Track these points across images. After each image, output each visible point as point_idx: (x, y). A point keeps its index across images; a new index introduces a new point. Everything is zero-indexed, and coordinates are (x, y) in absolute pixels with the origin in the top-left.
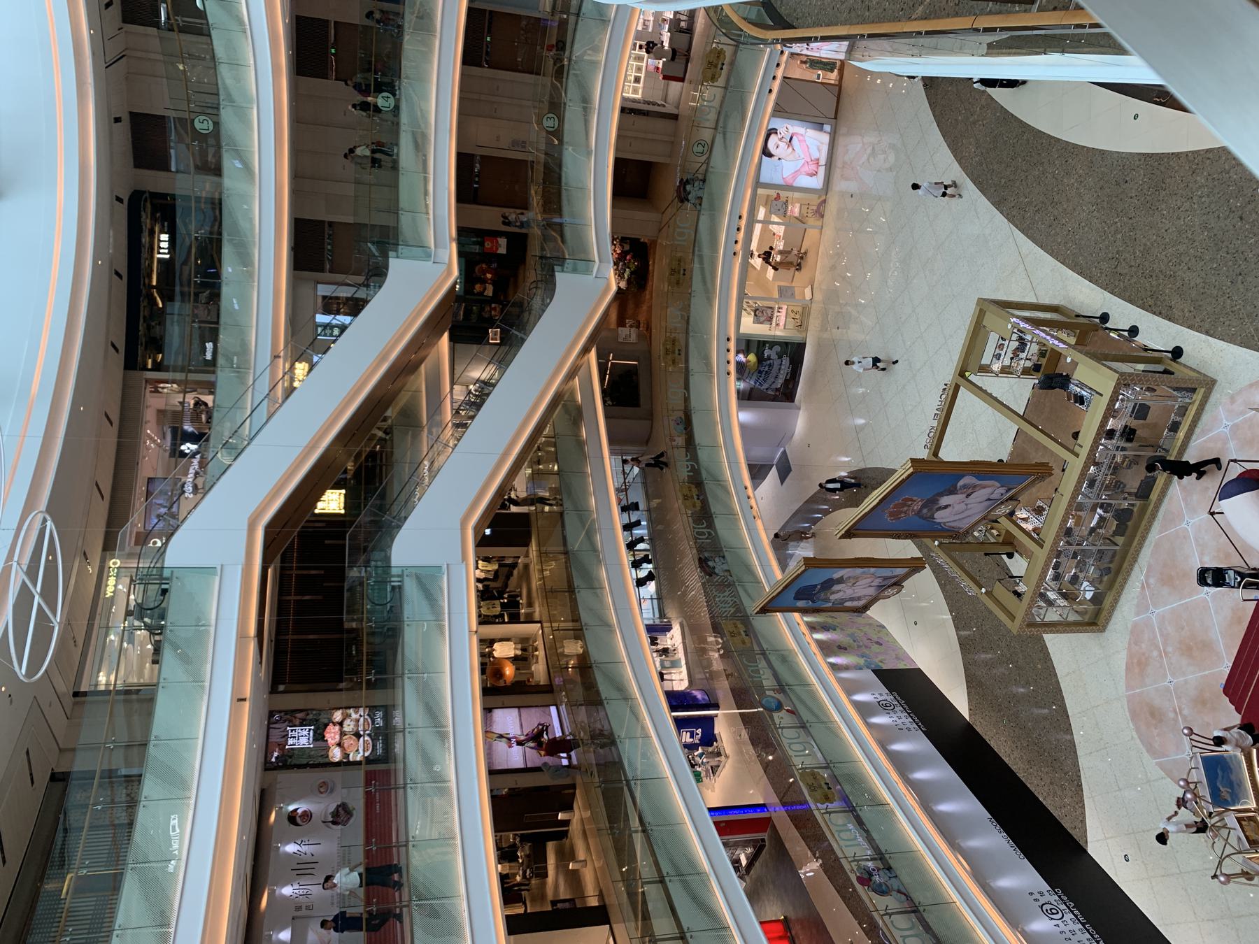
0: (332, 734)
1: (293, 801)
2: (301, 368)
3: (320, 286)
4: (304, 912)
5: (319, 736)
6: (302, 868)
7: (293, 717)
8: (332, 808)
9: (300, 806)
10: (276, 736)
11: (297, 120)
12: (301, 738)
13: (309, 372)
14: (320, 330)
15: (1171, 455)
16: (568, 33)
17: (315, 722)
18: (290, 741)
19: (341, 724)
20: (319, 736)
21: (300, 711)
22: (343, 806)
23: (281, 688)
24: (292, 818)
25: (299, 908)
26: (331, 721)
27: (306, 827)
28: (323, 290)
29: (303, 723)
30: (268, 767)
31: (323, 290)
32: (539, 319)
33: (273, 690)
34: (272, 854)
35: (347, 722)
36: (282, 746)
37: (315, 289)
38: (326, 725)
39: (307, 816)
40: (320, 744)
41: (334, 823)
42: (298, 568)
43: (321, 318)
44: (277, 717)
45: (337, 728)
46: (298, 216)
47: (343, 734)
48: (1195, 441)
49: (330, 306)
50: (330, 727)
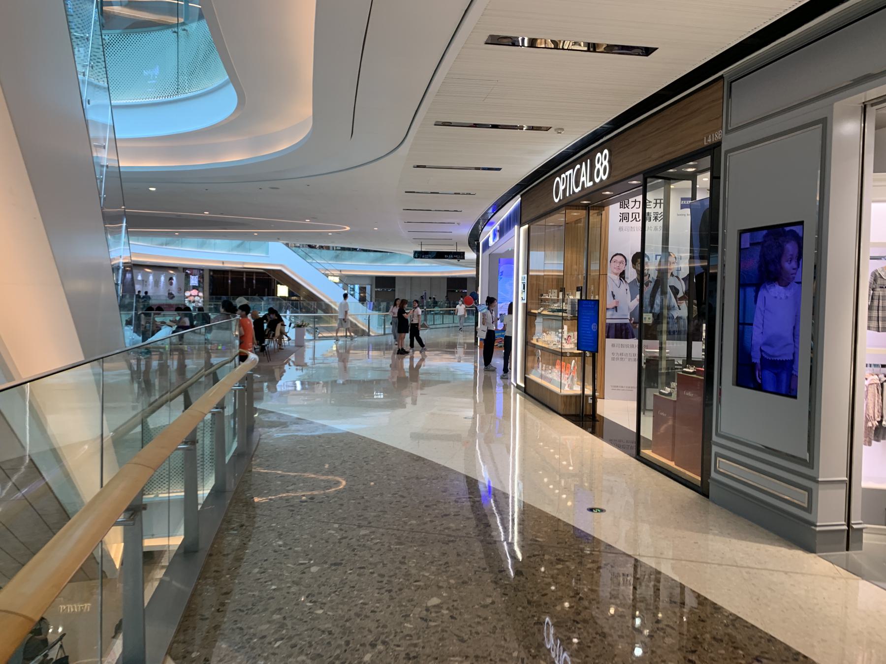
0: (194, 292)
1: (177, 279)
2: (337, 280)
3: (370, 286)
4: (145, 283)
5: (194, 288)
6: (157, 283)
7: (201, 277)
8: (173, 293)
9: (174, 281)
10: (195, 272)
11: (431, 279)
12: (194, 281)
13: (336, 283)
14: (352, 286)
15: (661, 369)
16: (725, 454)
17: (199, 286)
18: (193, 277)
19: (198, 296)
20: (194, 288)
21: (203, 281)
22: (174, 297)
23: (211, 274)
24: (171, 279)
25: (146, 282)
26: (199, 292)
27: (168, 283)
28: (368, 288)
29: (199, 282)
30: (185, 269)
31: (368, 288)
32: (424, 459)
33: (210, 270)
34: (161, 272)
35: (199, 298)
36: (191, 274)
37: (368, 285)
38: (197, 290)
39: (171, 284)
40: (191, 288)
41: (169, 294)
42: (120, 249)
43: (357, 287)
44: (201, 272)
45: (197, 294)
46: (396, 279)
47: (195, 296)
48: (855, 554)
49: (363, 290)
50: (197, 292)
